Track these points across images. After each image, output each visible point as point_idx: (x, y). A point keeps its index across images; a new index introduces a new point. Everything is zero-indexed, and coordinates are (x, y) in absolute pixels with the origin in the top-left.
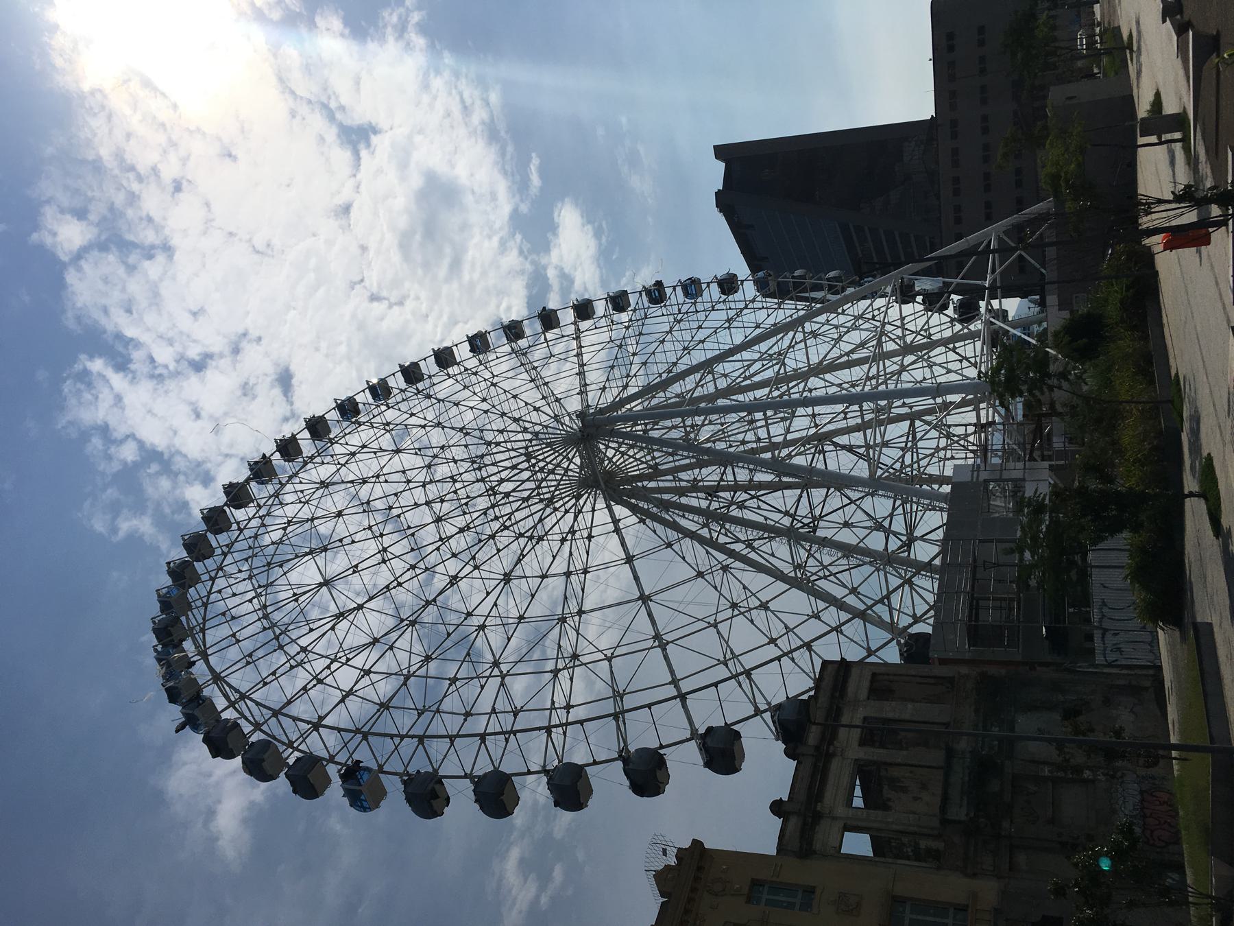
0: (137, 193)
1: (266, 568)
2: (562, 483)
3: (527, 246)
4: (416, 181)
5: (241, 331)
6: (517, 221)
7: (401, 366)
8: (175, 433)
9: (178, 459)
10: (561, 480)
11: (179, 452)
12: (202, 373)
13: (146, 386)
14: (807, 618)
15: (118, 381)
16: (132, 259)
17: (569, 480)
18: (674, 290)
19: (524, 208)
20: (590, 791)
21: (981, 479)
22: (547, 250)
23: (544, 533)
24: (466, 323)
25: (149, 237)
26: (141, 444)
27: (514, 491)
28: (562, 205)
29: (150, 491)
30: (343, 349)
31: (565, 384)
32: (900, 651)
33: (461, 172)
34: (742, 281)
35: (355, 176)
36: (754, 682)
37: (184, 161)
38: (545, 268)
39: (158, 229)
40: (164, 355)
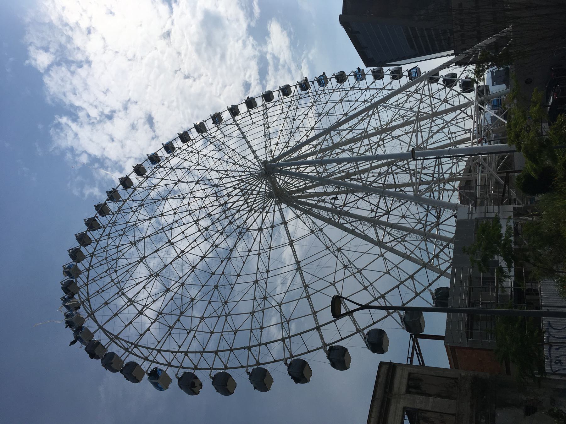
0: (71, 36)
2: (257, 199)
3: (255, 43)
4: (200, 16)
5: (127, 99)
6: (251, 31)
7: (179, 134)
8: (104, 149)
9: (107, 161)
10: (256, 197)
11: (107, 158)
12: (112, 120)
13: (88, 128)
14: (383, 273)
15: (74, 126)
16: (73, 68)
17: (261, 199)
18: (313, 83)
19: (253, 24)
20: (272, 381)
21: (474, 218)
22: (265, 43)
24: (230, 85)
25: (79, 57)
26: (89, 155)
28: (271, 22)
29: (96, 175)
30: (175, 104)
31: (257, 142)
32: (433, 297)
33: (221, 9)
34: (348, 76)
35: (171, 17)
37: (91, 18)
38: (266, 53)
39: (83, 52)
40: (94, 113)
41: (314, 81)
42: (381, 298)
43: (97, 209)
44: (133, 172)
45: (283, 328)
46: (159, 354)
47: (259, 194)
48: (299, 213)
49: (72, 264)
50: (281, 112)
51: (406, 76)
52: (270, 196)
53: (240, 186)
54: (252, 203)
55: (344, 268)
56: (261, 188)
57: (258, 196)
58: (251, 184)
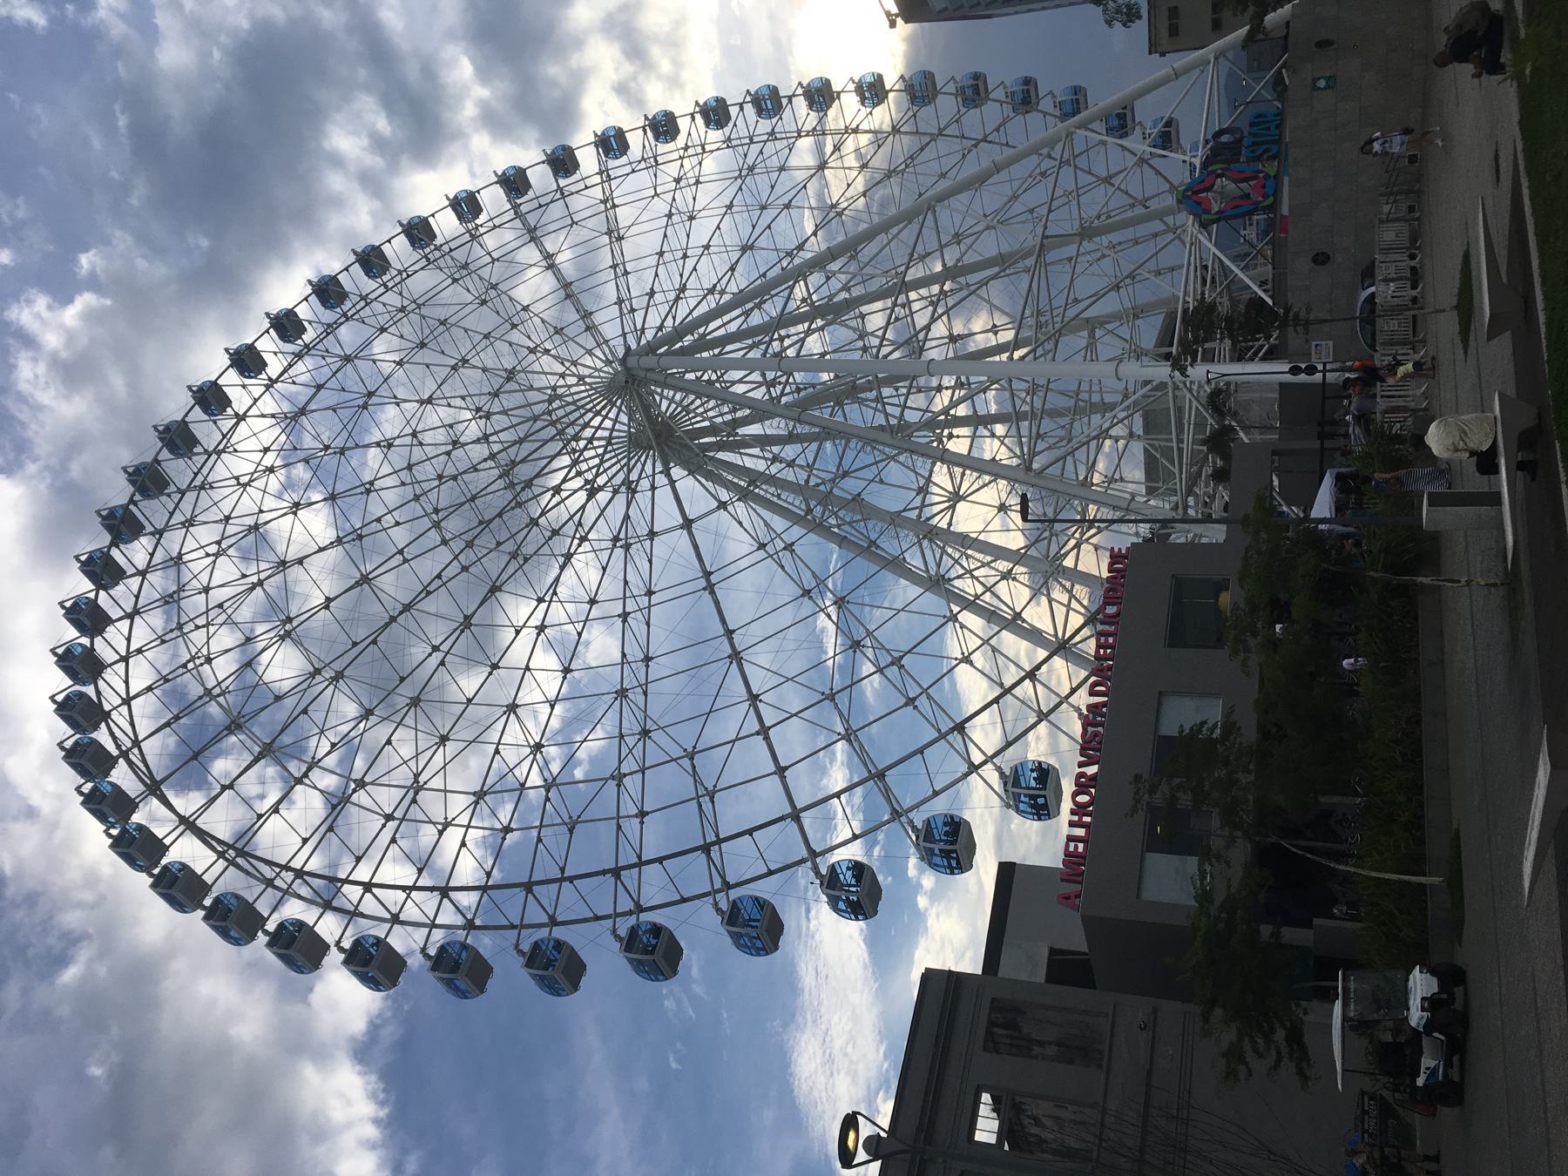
1: (437, 483)
2: (607, 456)
10: (605, 452)
18: (742, 109)
23: (708, 297)
34: (839, 93)
42: (956, 732)
44: (231, 366)
45: (704, 818)
46: (368, 895)
47: (612, 444)
48: (724, 495)
49: (80, 644)
50: (653, 193)
51: (1001, 103)
52: (636, 443)
53: (554, 417)
54: (594, 471)
57: (609, 448)
58: (582, 407)
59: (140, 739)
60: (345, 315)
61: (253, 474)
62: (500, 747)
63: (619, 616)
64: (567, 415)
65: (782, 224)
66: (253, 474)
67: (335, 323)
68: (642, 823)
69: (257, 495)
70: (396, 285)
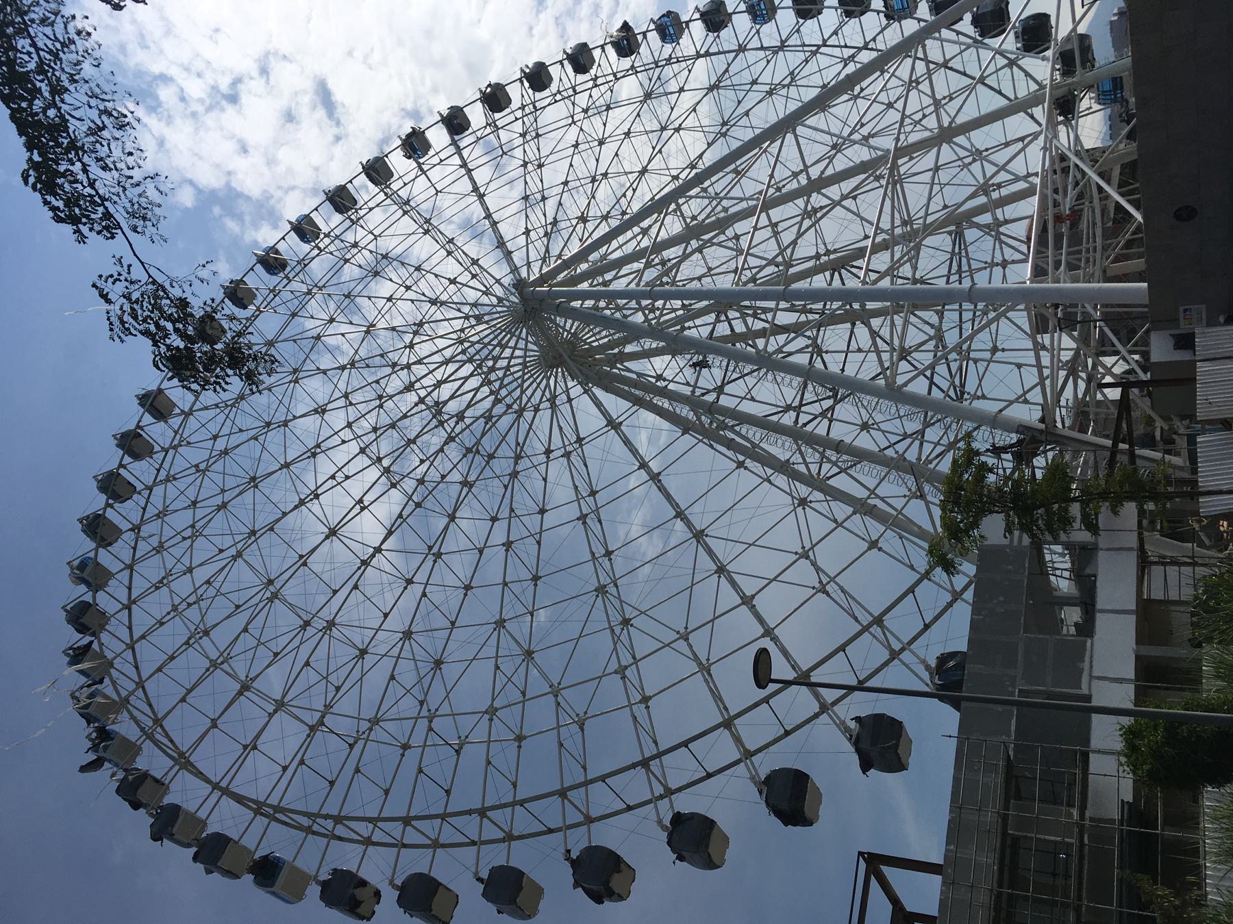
2: (526, 377)
18: (603, 50)
26: (199, 191)
27: (469, 406)
34: (687, 23)
36: (853, 598)
40: (196, 89)
41: (647, 31)
43: (142, 405)
46: (408, 828)
47: (527, 367)
55: (716, 572)
56: (515, 348)
58: (489, 343)
59: (160, 716)
60: (258, 309)
61: (208, 460)
62: (522, 699)
63: (578, 519)
64: (478, 352)
65: (626, 149)
66: (208, 460)
67: (253, 316)
68: (647, 707)
69: (218, 478)
70: (297, 274)
